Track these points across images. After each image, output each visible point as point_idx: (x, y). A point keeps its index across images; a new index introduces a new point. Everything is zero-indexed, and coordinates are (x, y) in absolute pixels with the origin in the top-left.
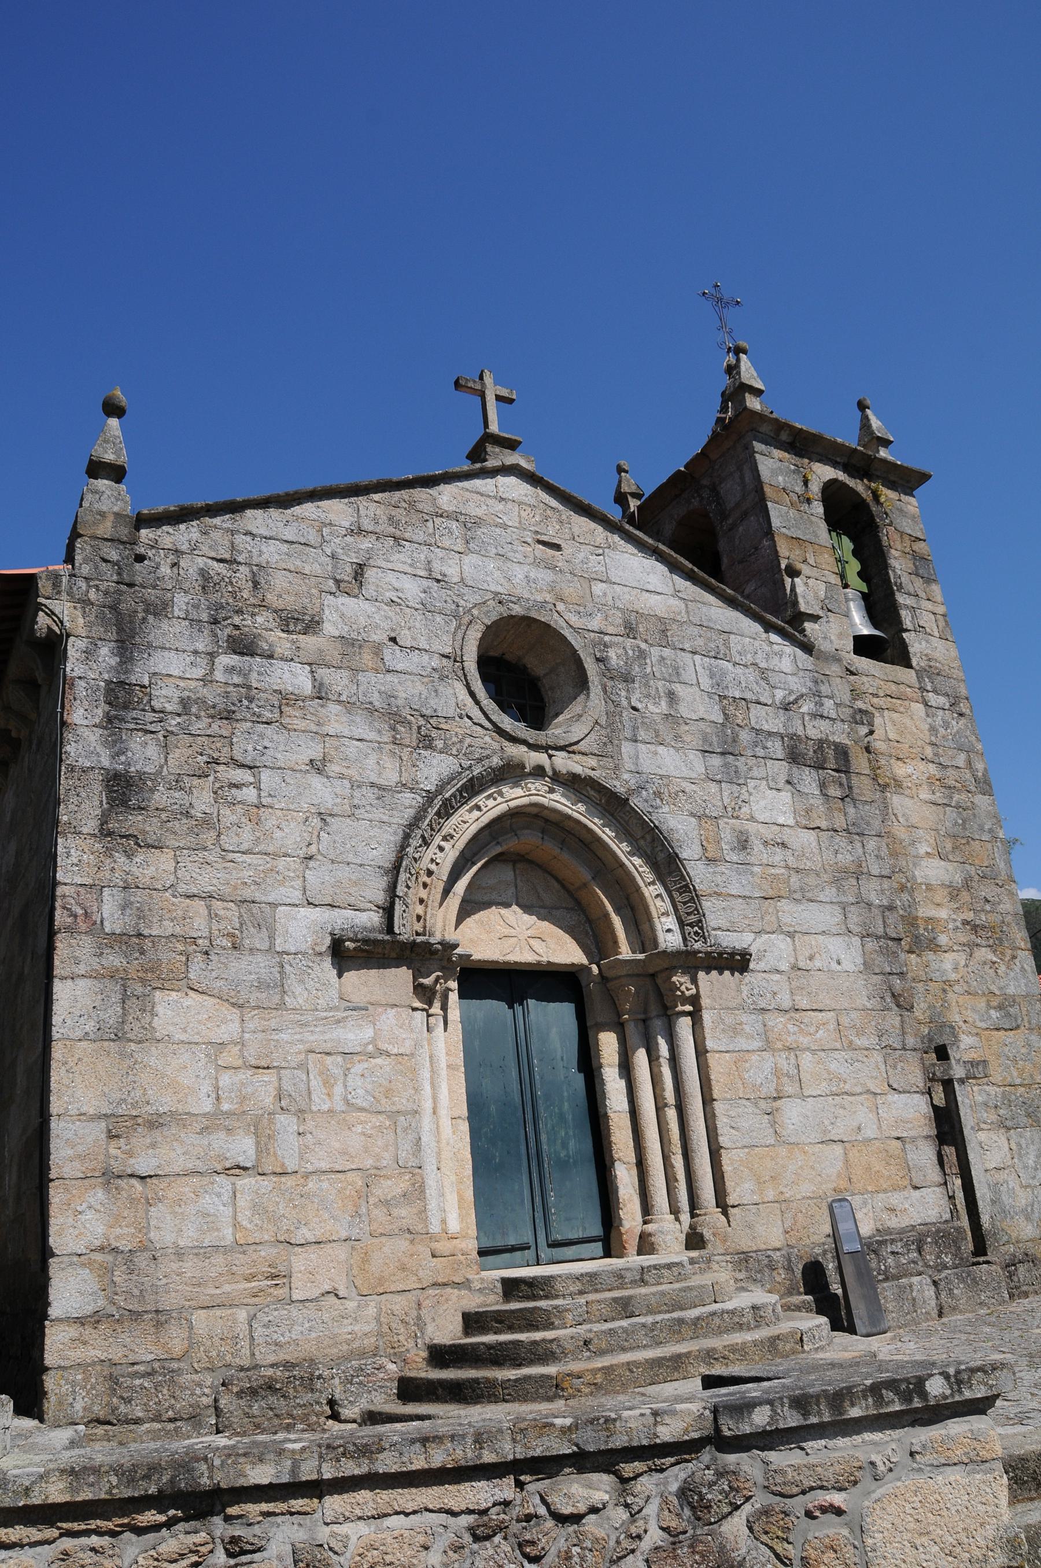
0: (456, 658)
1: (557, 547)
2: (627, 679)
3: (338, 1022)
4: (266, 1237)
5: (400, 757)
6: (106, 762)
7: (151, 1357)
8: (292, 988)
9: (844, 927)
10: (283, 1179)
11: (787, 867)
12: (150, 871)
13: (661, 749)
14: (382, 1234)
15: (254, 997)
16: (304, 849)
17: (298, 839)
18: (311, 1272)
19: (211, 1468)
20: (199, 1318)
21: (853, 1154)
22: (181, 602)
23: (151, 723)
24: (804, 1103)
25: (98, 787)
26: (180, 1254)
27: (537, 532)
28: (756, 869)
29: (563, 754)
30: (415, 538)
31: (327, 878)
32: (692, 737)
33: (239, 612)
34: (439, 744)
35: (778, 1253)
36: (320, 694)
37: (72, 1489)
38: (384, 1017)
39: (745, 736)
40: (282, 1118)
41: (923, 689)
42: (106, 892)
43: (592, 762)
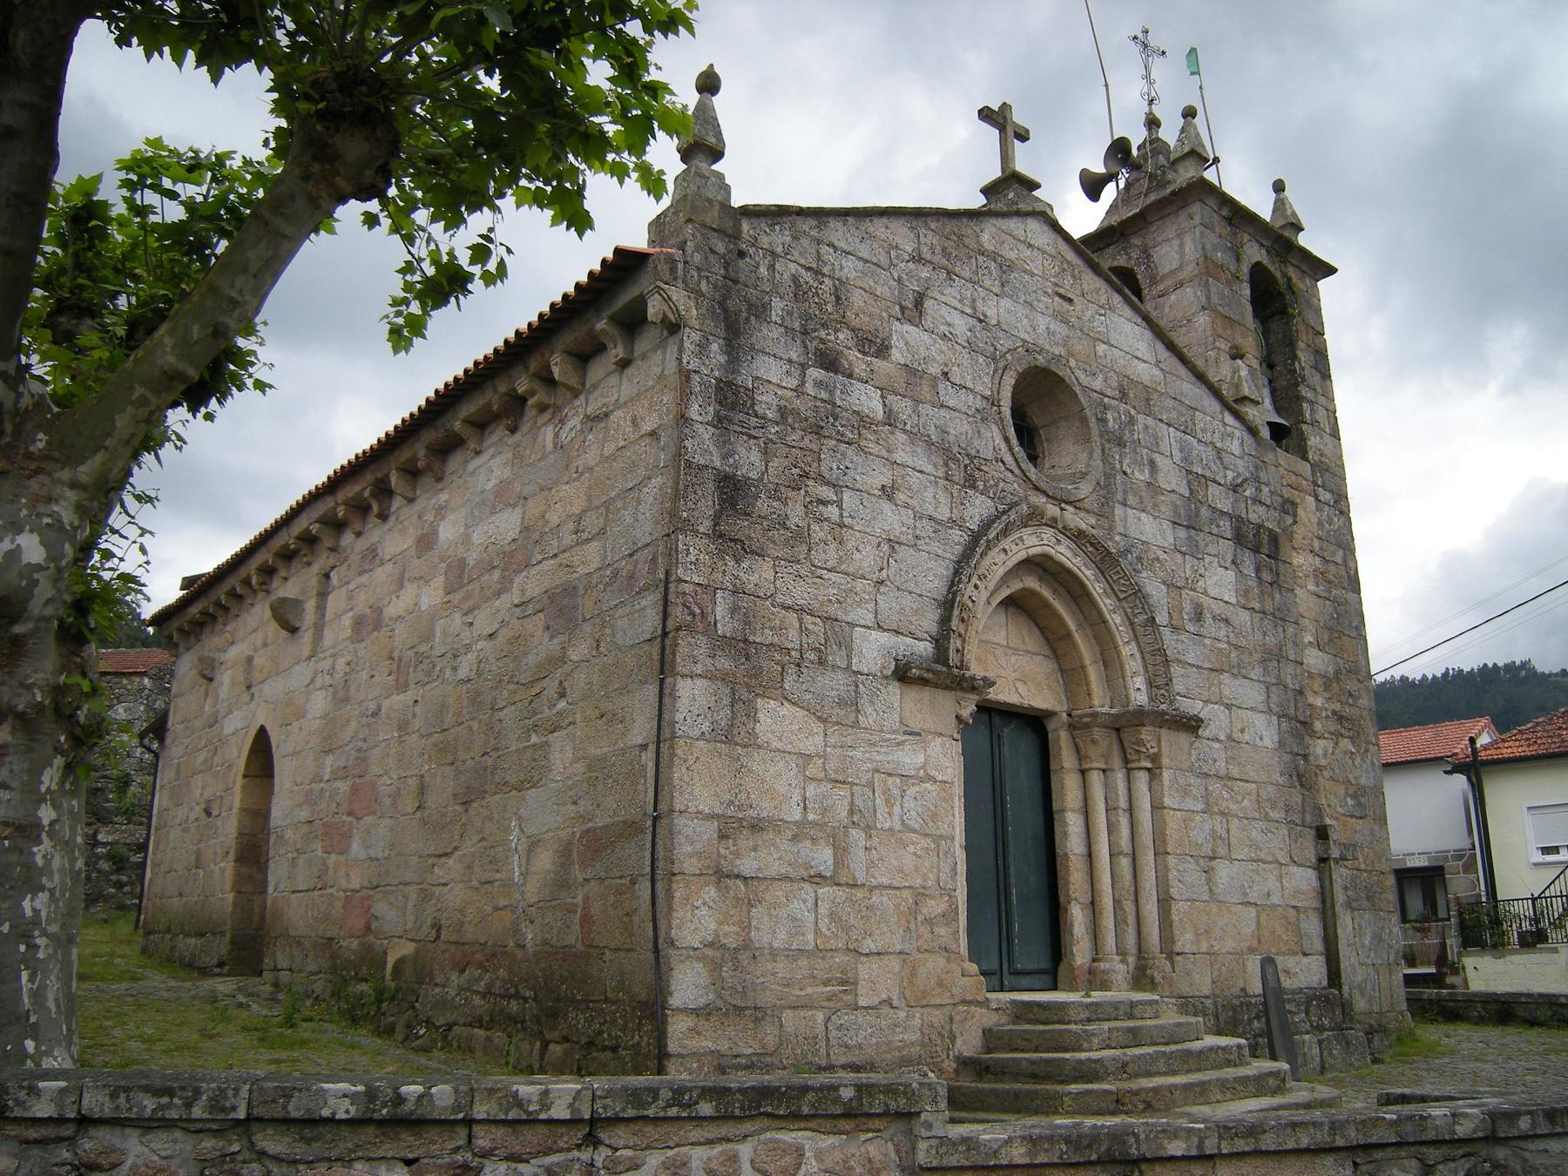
0: (993, 401)
1: (1070, 300)
2: (1121, 443)
3: (899, 744)
6: (718, 464)
7: (750, 1051)
11: (1228, 643)
12: (754, 578)
18: (877, 980)
19: (1138, 1141)
20: (787, 1015)
21: (1263, 917)
22: (778, 306)
25: (711, 486)
26: (774, 954)
27: (1056, 285)
30: (963, 274)
32: (1166, 504)
33: (824, 325)
34: (980, 484)
36: (890, 420)
37: (1030, 1153)
39: (1204, 512)
40: (853, 832)
41: (1315, 484)
42: (719, 594)
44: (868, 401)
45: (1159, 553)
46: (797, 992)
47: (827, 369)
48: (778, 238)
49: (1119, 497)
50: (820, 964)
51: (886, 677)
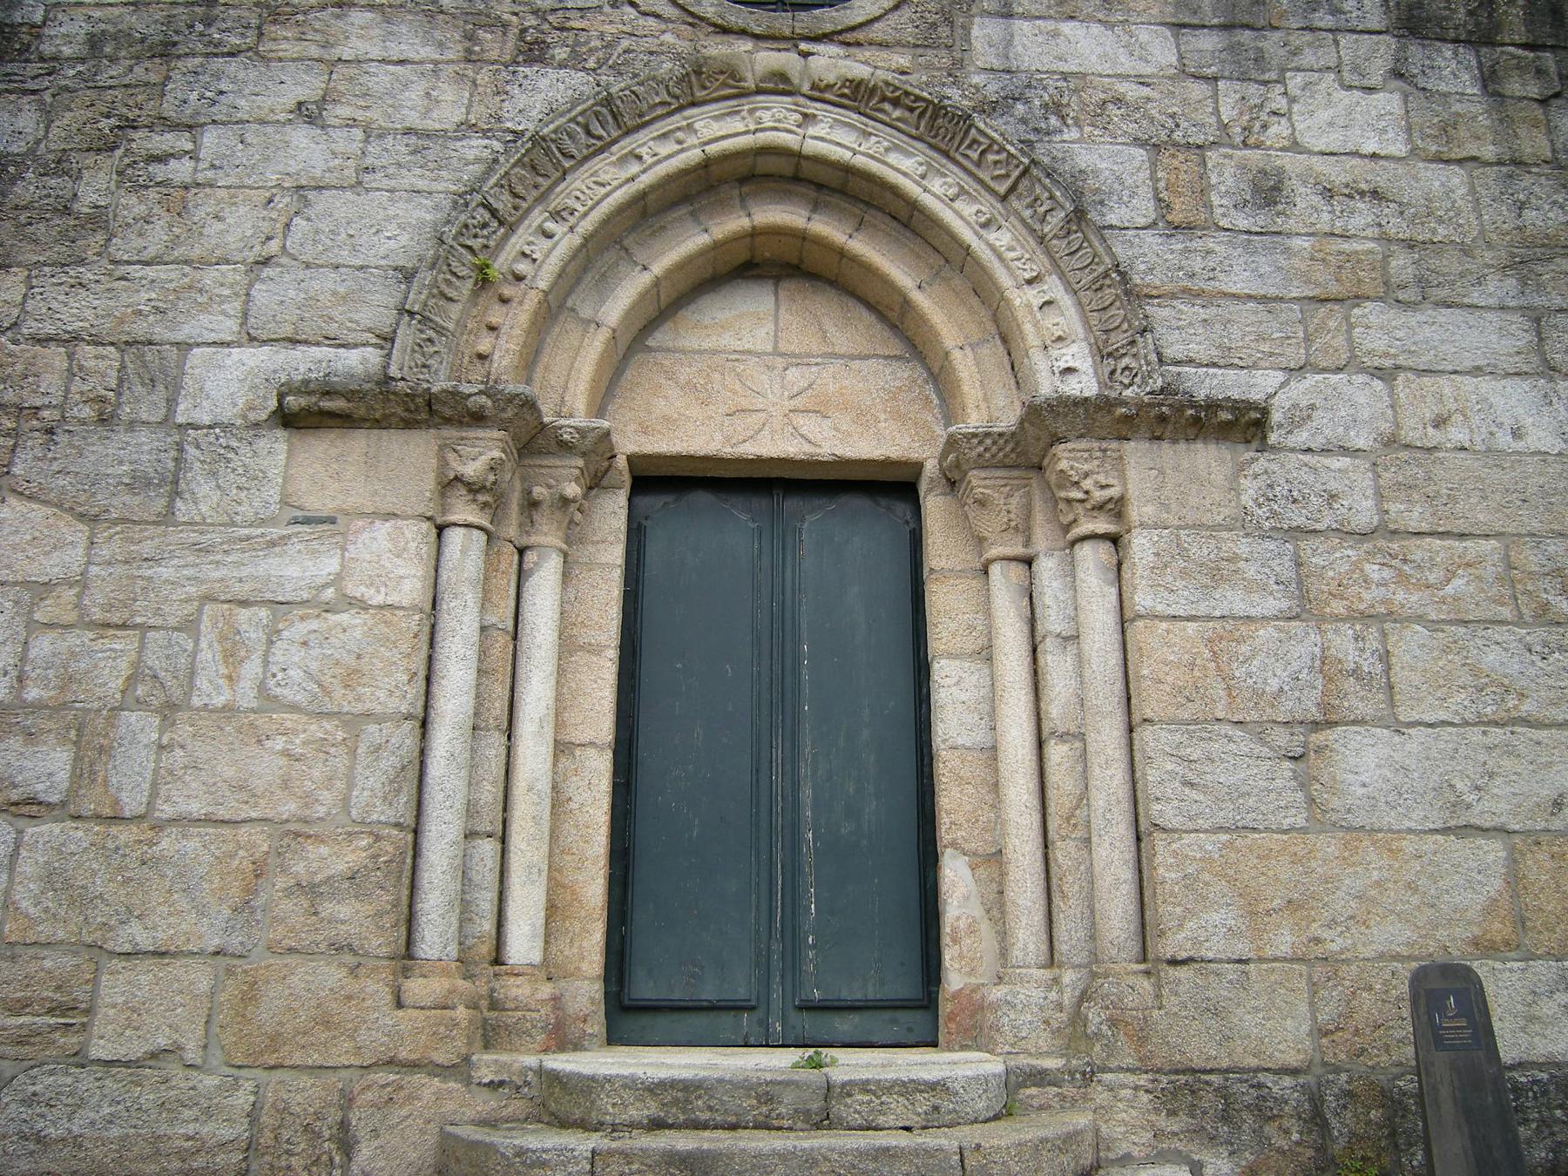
3: (272, 544)
4: (61, 934)
5: (474, 82)
8: (193, 485)
9: (1535, 359)
10: (114, 830)
13: (1067, 28)
14: (291, 950)
15: (122, 503)
16: (258, 248)
17: (249, 233)
23: (33, 78)
24: (1397, 739)
28: (1297, 243)
29: (833, 49)
31: (292, 293)
35: (1288, 1081)
38: (365, 535)
43: (902, 60)
45: (1123, 88)
51: (257, 425)
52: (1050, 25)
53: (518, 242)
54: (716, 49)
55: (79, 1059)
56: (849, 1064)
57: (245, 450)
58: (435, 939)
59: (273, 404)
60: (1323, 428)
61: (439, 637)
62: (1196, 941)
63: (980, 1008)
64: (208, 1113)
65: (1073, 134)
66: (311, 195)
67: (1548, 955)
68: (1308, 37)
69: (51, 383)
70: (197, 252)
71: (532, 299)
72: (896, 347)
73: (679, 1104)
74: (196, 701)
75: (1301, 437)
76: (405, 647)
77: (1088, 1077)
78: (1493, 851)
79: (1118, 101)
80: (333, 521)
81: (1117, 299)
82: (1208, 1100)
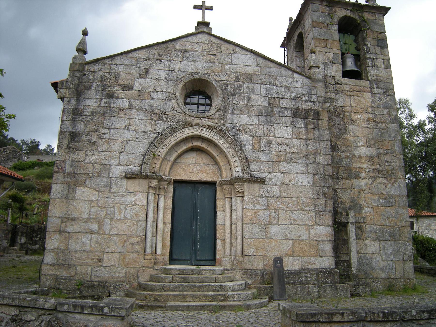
1: (215, 55)
3: (125, 196)
9: (306, 171)
12: (78, 157)
13: (242, 116)
22: (94, 85)
25: (68, 136)
26: (76, 251)
29: (206, 119)
33: (110, 86)
35: (259, 271)
42: (67, 162)
44: (125, 103)
45: (249, 126)
46: (82, 261)
47: (109, 98)
48: (96, 67)
49: (230, 111)
50: (91, 254)
51: (122, 178)
52: (239, 116)
53: (159, 150)
54: (189, 119)
55: (102, 266)
56: (203, 268)
57: (120, 182)
58: (148, 251)
59: (124, 175)
60: (273, 182)
61: (148, 209)
62: (249, 253)
63: (221, 261)
64: (120, 273)
65: (241, 134)
66: (128, 142)
67: (296, 256)
68: (279, 118)
69: (90, 170)
70: (111, 150)
71: (161, 159)
72: (214, 163)
73: (182, 271)
74: (115, 218)
75: (270, 183)
76: (144, 211)
77: (233, 270)
78: (290, 242)
79: (248, 129)
80: (133, 192)
81: (246, 161)
82: (249, 273)
